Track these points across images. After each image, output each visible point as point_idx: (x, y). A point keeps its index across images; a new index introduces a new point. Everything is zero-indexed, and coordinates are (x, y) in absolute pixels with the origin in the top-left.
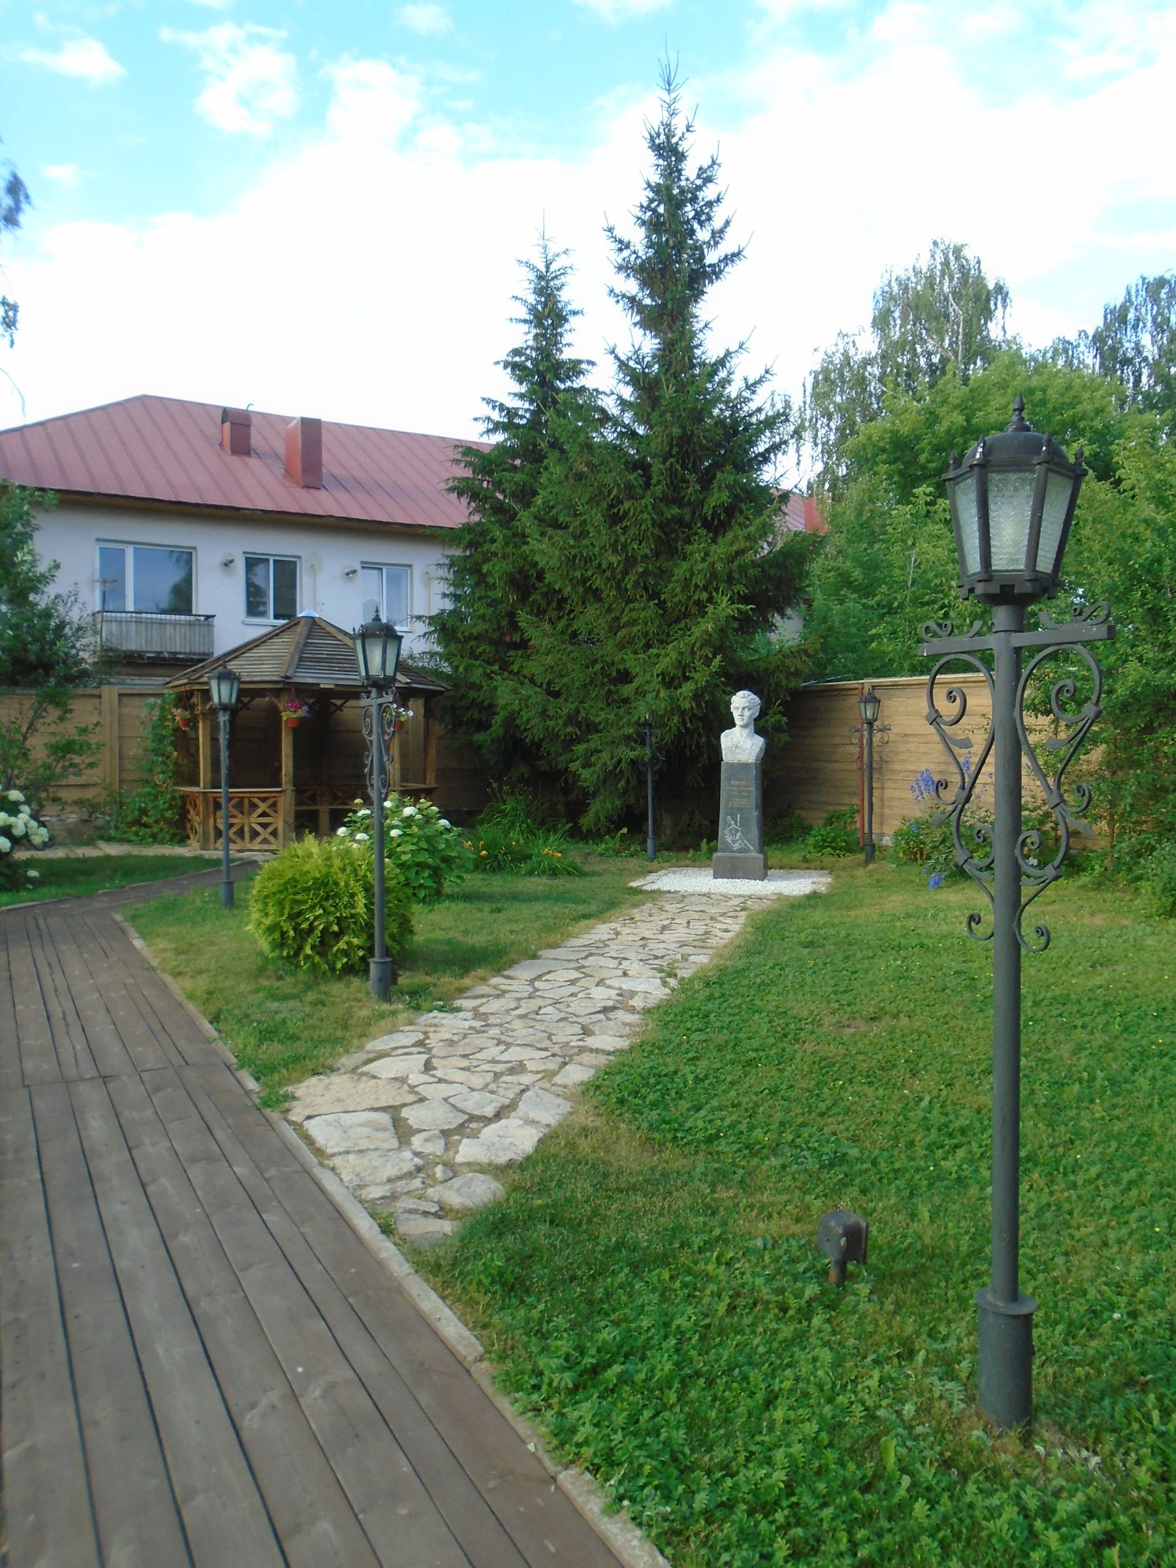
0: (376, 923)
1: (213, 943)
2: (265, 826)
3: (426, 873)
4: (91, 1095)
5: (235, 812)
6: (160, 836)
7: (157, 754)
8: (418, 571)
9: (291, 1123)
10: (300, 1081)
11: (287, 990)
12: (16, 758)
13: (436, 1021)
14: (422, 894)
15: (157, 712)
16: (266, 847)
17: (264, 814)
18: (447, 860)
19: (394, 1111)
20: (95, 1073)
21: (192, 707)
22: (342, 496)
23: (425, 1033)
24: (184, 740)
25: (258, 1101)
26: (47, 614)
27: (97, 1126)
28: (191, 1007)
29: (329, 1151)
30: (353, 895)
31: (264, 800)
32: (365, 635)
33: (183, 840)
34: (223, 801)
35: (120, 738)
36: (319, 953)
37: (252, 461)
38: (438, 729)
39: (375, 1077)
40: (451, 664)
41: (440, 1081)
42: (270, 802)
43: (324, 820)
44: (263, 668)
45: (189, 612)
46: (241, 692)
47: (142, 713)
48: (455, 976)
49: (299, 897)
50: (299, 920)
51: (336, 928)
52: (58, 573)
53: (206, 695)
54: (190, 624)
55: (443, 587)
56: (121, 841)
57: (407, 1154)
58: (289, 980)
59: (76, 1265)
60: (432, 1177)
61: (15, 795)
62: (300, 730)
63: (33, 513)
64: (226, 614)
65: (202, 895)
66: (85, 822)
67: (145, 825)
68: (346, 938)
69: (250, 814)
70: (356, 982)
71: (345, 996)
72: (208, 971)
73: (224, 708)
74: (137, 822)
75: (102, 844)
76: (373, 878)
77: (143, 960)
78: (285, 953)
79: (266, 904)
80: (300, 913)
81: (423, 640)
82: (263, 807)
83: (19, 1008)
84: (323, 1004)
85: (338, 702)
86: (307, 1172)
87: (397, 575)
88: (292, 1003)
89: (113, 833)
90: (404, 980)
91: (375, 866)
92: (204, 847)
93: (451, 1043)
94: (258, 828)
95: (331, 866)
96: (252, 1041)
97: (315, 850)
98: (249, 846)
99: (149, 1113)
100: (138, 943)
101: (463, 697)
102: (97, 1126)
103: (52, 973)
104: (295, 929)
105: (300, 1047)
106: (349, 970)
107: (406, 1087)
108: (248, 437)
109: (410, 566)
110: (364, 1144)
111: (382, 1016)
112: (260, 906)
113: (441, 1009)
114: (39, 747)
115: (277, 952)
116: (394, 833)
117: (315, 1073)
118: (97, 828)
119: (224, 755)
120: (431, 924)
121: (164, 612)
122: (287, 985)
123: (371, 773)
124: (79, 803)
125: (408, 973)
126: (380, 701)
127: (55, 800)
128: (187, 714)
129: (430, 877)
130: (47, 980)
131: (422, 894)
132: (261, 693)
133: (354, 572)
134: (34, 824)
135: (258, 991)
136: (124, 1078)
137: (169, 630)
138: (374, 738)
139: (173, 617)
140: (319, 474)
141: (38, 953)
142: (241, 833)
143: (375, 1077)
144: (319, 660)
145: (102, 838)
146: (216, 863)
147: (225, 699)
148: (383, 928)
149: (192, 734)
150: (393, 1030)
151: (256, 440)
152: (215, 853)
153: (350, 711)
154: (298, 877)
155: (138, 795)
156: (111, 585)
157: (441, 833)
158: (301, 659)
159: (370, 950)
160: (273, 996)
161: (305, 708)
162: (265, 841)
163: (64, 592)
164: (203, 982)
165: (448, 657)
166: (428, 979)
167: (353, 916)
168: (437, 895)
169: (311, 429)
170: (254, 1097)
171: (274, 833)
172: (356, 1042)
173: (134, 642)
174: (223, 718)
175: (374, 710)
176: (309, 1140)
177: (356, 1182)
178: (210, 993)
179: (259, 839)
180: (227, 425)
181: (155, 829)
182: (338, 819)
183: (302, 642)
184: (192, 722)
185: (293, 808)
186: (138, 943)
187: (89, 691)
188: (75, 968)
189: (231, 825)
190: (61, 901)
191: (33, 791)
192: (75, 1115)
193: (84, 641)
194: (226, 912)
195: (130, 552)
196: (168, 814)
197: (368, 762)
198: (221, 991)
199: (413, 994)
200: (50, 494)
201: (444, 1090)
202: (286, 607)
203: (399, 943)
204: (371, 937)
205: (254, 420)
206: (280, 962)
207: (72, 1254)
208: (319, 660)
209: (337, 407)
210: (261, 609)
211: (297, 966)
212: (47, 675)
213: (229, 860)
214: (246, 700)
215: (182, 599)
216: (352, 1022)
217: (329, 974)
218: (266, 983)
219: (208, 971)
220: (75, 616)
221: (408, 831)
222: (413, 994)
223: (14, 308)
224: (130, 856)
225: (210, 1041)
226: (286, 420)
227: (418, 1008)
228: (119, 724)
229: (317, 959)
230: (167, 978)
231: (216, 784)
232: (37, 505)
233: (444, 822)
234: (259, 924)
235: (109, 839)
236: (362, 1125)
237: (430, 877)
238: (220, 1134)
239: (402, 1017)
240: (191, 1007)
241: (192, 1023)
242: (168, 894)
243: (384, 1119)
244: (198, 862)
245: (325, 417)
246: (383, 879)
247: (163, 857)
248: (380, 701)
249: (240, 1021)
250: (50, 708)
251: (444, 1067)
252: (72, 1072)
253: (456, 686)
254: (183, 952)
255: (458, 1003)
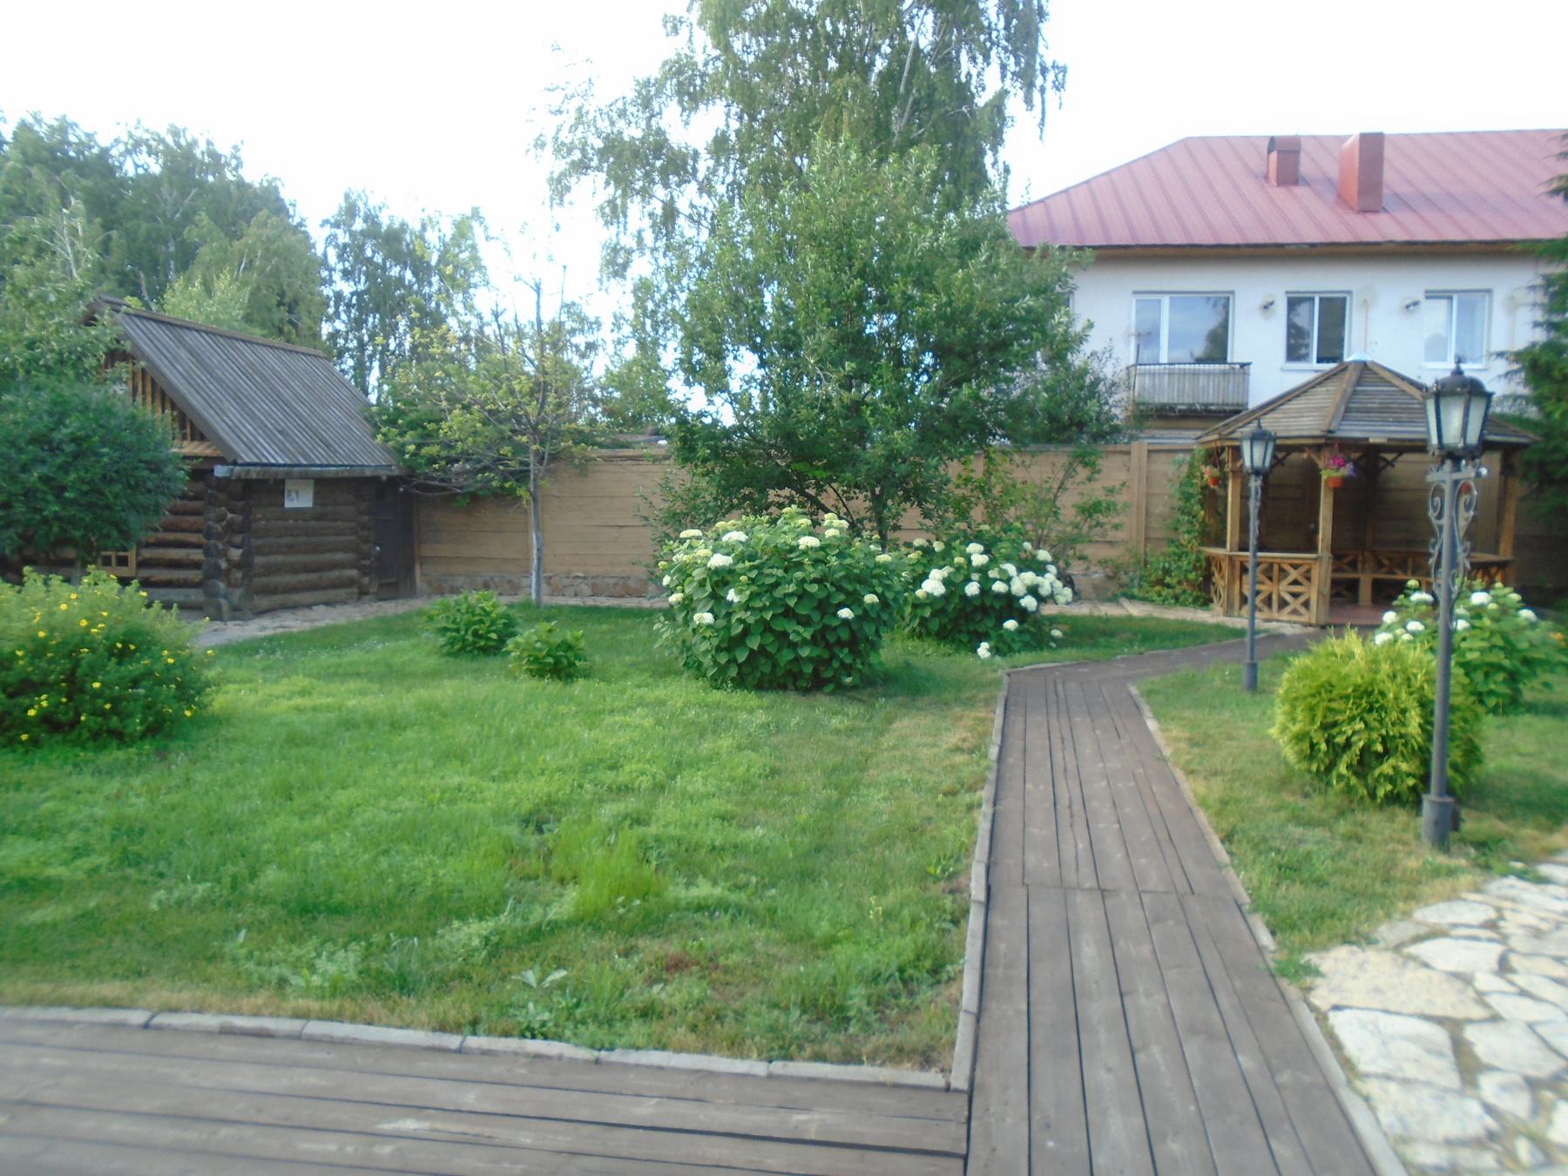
0: (1435, 749)
1: (1230, 738)
2: (1295, 595)
3: (1500, 676)
4: (1087, 910)
5: (1261, 577)
6: (1182, 598)
7: (1183, 513)
8: (1499, 296)
9: (1313, 1009)
10: (1325, 948)
11: (1315, 813)
12: (1047, 516)
13: (1513, 893)
14: (1492, 702)
15: (1185, 469)
16: (1295, 618)
17: (1295, 582)
18: (1527, 662)
19: (1453, 1026)
20: (1094, 884)
21: (1221, 464)
22: (1407, 218)
23: (1499, 910)
24: (1212, 500)
25: (1272, 965)
26: (1084, 372)
27: (1090, 954)
28: (1202, 816)
29: (1363, 1067)
30: (1404, 711)
31: (1295, 567)
32: (1441, 393)
33: (1206, 603)
34: (1250, 566)
35: (1148, 495)
36: (1356, 774)
37: (1300, 191)
38: (1519, 488)
39: (1426, 965)
40: (1541, 409)
41: (1523, 993)
42: (1302, 569)
43: (1365, 591)
44: (1303, 423)
45: (1223, 360)
46: (1277, 448)
47: (1169, 471)
48: (1539, 827)
49: (1334, 705)
50: (1334, 731)
51: (1379, 748)
52: (1091, 333)
53: (1237, 451)
54: (1224, 373)
55: (1539, 316)
56: (1144, 600)
57: (1474, 1107)
58: (1317, 799)
59: (1051, 1144)
60: (1511, 1154)
61: (1043, 555)
62: (1342, 491)
63: (1070, 273)
64: (1266, 366)
65: (1223, 673)
66: (1109, 577)
67: (1168, 586)
68: (1392, 761)
69: (1279, 581)
70: (1402, 815)
71: (1387, 833)
72: (1223, 773)
73: (1257, 472)
74: (1160, 582)
75: (1125, 602)
76: (1434, 694)
77: (1156, 749)
78: (1314, 768)
79: (1294, 708)
80: (1335, 724)
81: (1503, 381)
82: (1294, 574)
83: (1029, 786)
84: (1359, 840)
85: (1389, 457)
86: (1331, 1090)
87: (1470, 304)
88: (1319, 833)
89: (1136, 591)
90: (1472, 824)
91: (1438, 676)
92: (1228, 612)
93: (1537, 934)
94: (1288, 598)
95: (1377, 672)
96: (1269, 880)
97: (1358, 649)
98: (1276, 615)
99: (1146, 950)
100: (1152, 725)
101: (1556, 449)
102: (1090, 954)
103: (1063, 749)
104: (1328, 742)
105: (1326, 898)
106: (1394, 799)
107: (1471, 993)
108: (1297, 163)
109: (1489, 291)
110: (1411, 1071)
111: (1437, 872)
112: (1287, 707)
113: (1521, 875)
114: (1068, 503)
115: (1304, 765)
116: (1461, 625)
117: (1346, 941)
118: (1121, 586)
119: (1254, 524)
120: (1511, 747)
121: (1199, 361)
122: (1314, 806)
123: (1438, 565)
124: (1103, 563)
125: (1474, 813)
126: (1456, 476)
127: (1081, 558)
128: (1216, 472)
129: (1507, 682)
130: (1058, 756)
131: (1492, 702)
132: (1300, 448)
133: (1416, 304)
134: (1059, 584)
135: (1278, 809)
136: (1123, 896)
137: (1202, 381)
138: (1445, 521)
139: (1212, 367)
140: (1379, 196)
141: (1054, 721)
142: (1268, 601)
143: (1426, 965)
144: (1368, 411)
145: (1125, 595)
146: (1238, 633)
147: (1258, 462)
148: (1444, 754)
149: (1220, 492)
150: (1453, 896)
151: (1306, 167)
152: (1240, 622)
153: (1404, 468)
154: (1334, 681)
155: (1164, 554)
156: (1147, 337)
157: (1524, 628)
158: (1347, 410)
159: (1425, 779)
160: (1297, 819)
161: (1350, 466)
162: (1295, 612)
163: (1099, 348)
164: (1218, 787)
165: (1538, 401)
166: (1502, 827)
167: (1402, 736)
168: (1512, 704)
169: (1372, 145)
170: (1269, 957)
171: (1306, 604)
172: (1401, 905)
173: (1167, 394)
174: (1255, 484)
175: (1447, 488)
176: (1337, 1045)
177: (1399, 1130)
178: (1224, 803)
179: (1288, 609)
180: (1274, 155)
181: (1178, 590)
182: (1387, 594)
183: (1350, 390)
184: (1221, 481)
185: (1330, 575)
186: (1152, 725)
187: (1119, 447)
188: (1087, 749)
189: (1258, 593)
190: (1080, 665)
191: (1063, 548)
192: (1069, 933)
193: (1117, 397)
194: (1247, 696)
195: (1166, 300)
196: (1192, 576)
197: (1435, 552)
198: (1238, 801)
199: (1481, 845)
200: (1089, 252)
201: (1526, 1010)
202: (1331, 348)
203: (1463, 774)
204: (1426, 763)
205: (1305, 145)
206: (1308, 777)
207: (1048, 1126)
208: (1368, 411)
209: (1396, 118)
210: (1303, 351)
211: (1329, 784)
212: (1081, 431)
213: (1254, 632)
214: (1280, 455)
215: (1217, 346)
216: (1397, 873)
217: (1368, 800)
218: (1291, 799)
219: (1223, 773)
220: (1108, 371)
221: (1477, 623)
222: (1481, 845)
223: (1064, 70)
224: (1149, 618)
225: (1220, 867)
226: (1341, 139)
227: (1487, 867)
228: (1142, 482)
229: (1354, 780)
230: (1179, 774)
231: (1243, 547)
232: (1075, 264)
233: (1527, 614)
234: (1284, 729)
235: (1132, 597)
236: (1407, 1038)
237: (1507, 682)
238: (1225, 1001)
239: (1465, 880)
240: (1202, 816)
241: (1201, 836)
242: (1186, 669)
243: (1440, 1036)
244: (1223, 632)
245: (1387, 129)
246: (1446, 693)
247: (1183, 622)
248: (1456, 476)
249: (1255, 846)
250: (1080, 469)
251: (1529, 972)
252: (1071, 877)
253: (1547, 436)
254: (1197, 745)
255: (1545, 869)
